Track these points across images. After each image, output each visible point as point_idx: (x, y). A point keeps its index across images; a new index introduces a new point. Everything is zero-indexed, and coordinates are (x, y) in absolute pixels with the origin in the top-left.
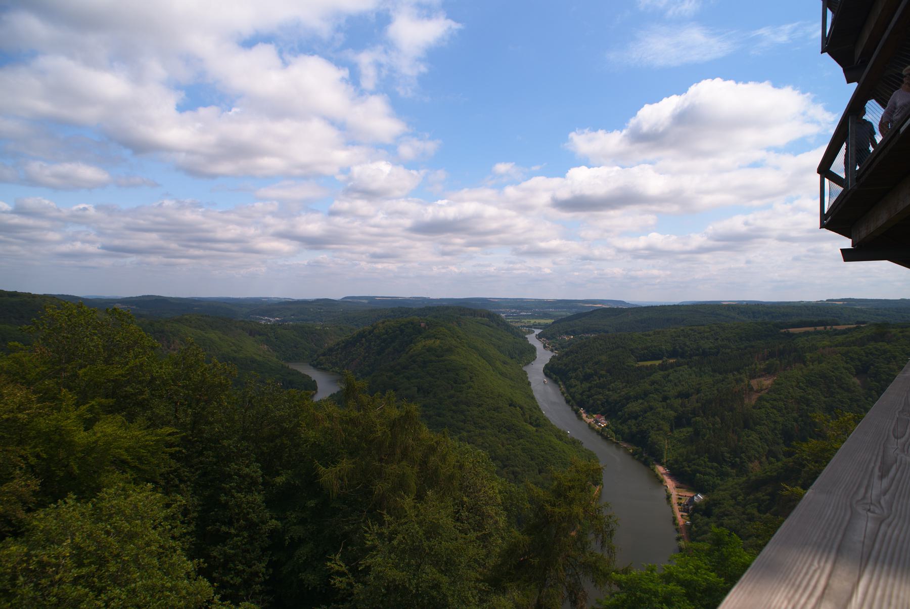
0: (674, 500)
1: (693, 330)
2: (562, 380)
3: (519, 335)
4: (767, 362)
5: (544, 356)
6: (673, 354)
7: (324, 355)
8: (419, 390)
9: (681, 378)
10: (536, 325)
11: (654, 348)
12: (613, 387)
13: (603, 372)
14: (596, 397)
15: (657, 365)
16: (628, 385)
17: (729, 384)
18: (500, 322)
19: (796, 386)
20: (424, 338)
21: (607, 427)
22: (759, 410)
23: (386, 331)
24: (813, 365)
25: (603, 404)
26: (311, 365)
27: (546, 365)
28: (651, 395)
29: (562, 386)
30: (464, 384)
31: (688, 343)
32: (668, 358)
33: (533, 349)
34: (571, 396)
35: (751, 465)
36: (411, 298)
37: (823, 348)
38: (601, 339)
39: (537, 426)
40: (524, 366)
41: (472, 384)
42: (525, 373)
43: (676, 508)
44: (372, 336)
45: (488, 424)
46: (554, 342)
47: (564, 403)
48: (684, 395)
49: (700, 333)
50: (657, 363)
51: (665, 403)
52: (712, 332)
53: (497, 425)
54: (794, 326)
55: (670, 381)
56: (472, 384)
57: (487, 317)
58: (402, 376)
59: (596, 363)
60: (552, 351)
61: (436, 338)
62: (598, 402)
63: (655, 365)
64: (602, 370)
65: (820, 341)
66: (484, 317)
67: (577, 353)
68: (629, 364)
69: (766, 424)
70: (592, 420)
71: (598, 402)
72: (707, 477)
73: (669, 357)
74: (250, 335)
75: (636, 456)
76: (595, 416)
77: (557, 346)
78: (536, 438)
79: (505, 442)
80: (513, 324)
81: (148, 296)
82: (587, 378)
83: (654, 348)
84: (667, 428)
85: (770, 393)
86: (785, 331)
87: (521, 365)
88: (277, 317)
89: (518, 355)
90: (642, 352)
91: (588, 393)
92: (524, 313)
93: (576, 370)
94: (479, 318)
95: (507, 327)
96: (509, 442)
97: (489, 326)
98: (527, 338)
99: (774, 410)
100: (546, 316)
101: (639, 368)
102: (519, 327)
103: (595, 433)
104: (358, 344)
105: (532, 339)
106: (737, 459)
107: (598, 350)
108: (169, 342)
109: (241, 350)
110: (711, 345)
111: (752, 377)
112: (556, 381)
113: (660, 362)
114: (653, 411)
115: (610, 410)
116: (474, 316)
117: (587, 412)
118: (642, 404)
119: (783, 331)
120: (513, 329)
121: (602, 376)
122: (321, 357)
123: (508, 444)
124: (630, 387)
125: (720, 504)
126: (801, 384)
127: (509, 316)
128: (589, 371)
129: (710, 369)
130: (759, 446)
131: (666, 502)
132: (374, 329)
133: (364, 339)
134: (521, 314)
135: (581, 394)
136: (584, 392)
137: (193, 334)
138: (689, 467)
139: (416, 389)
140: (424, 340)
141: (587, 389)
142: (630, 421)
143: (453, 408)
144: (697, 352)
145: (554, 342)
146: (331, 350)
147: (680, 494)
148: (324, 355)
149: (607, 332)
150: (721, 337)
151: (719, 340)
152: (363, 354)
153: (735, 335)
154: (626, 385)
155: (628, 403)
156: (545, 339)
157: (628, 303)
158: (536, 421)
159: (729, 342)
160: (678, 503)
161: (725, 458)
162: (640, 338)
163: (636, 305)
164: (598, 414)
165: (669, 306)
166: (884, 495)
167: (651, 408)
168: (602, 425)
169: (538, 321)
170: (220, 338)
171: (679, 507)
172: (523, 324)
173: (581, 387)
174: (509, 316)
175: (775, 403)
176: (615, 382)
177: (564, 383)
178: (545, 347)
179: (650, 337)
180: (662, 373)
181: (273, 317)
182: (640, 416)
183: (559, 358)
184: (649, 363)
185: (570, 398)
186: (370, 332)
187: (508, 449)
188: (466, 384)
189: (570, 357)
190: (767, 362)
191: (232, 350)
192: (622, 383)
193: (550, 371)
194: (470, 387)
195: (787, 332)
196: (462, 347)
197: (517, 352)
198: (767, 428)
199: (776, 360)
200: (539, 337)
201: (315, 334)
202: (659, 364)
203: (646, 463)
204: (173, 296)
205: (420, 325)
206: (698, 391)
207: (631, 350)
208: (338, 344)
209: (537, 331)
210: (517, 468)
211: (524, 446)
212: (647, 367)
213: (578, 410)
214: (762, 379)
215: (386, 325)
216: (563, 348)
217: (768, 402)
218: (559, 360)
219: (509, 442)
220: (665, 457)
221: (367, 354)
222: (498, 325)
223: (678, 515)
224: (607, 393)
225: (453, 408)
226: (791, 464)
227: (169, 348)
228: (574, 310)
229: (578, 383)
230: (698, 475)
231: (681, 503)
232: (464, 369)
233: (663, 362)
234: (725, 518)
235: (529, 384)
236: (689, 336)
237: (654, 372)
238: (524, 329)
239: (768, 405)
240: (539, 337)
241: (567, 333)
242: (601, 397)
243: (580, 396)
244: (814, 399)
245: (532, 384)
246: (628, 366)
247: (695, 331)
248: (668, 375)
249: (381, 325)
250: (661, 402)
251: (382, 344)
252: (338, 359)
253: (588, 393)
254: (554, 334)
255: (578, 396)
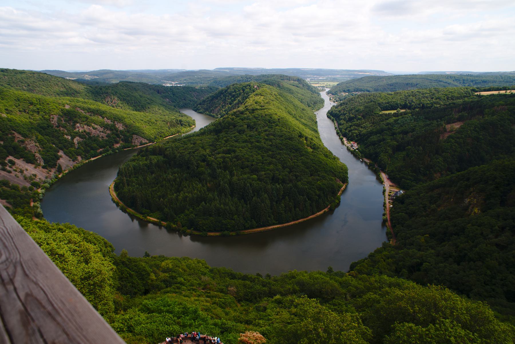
0: (387, 193)
1: (419, 92)
2: (336, 120)
3: (315, 92)
4: (460, 114)
5: (329, 105)
6: (404, 107)
7: (200, 104)
8: (248, 127)
9: (405, 122)
10: (327, 86)
11: (393, 103)
12: (364, 126)
13: (360, 117)
14: (353, 131)
15: (393, 113)
16: (373, 125)
17: (433, 127)
18: (305, 84)
19: (473, 130)
20: (255, 95)
21: (357, 149)
22: (447, 144)
23: (235, 90)
24: (488, 117)
25: (357, 136)
26: (193, 110)
27: (329, 111)
28: (385, 132)
29: (336, 124)
30: (274, 123)
31: (414, 101)
32: (400, 109)
33: (322, 101)
34: (340, 130)
35: (435, 175)
36: (255, 68)
37: (498, 106)
38: (362, 96)
39: (314, 148)
40: (316, 111)
41: (278, 123)
42: (315, 116)
43: (387, 197)
44: (227, 93)
45: (284, 147)
46: (336, 97)
47: (335, 134)
48: (405, 133)
49: (423, 94)
50: (393, 112)
51: (392, 137)
52: (431, 94)
53: (289, 148)
54: (485, 90)
55: (399, 124)
56: (278, 123)
57: (297, 81)
58: (239, 118)
59: (357, 111)
60: (334, 102)
61: (261, 95)
62: (355, 134)
63: (391, 113)
64: (359, 115)
65: (498, 101)
66: (295, 81)
67: (347, 104)
68: (375, 112)
69: (450, 152)
70: (350, 145)
71: (355, 134)
72: (408, 181)
73: (401, 109)
74: (159, 93)
75: (371, 167)
76: (351, 142)
77: (337, 99)
78: (311, 156)
79: (293, 158)
80: (312, 85)
81: (103, 70)
82: (350, 119)
83: (393, 103)
84: (390, 152)
85: (456, 134)
86: (477, 94)
87: (314, 110)
88: (176, 81)
89: (313, 105)
90: (385, 105)
91: (349, 129)
92: (321, 78)
93: (345, 115)
94: (292, 82)
95: (309, 88)
96: (295, 158)
97: (297, 87)
98: (320, 94)
99: (456, 144)
100: (334, 80)
101: (381, 115)
102: (317, 87)
103: (350, 153)
104: (219, 98)
105: (324, 95)
106: (428, 172)
107: (359, 103)
108: (111, 99)
109: (153, 103)
110: (428, 102)
111: (448, 123)
112: (333, 121)
113: (395, 111)
114: (384, 141)
115: (360, 139)
116: (289, 81)
117: (348, 140)
118: (379, 137)
119: (476, 94)
120: (312, 89)
121: (359, 119)
122: (199, 106)
123: (294, 159)
124: (374, 126)
125: (410, 197)
126: (477, 129)
127: (312, 80)
128: (352, 115)
129: (424, 117)
130: (442, 165)
131: (382, 194)
132: (228, 89)
133: (222, 95)
134: (320, 78)
135: (346, 129)
136: (347, 128)
137: (124, 94)
138: (399, 175)
139: (246, 126)
140: (254, 96)
141: (349, 127)
142: (370, 146)
143: (266, 137)
144: (419, 106)
145: (336, 97)
146: (204, 101)
147: (391, 190)
148: (200, 104)
149: (369, 91)
150: (436, 97)
151: (434, 99)
152: (222, 104)
153: (444, 96)
154: (372, 125)
155: (371, 136)
156: (331, 95)
157: (386, 72)
158: (313, 146)
159: (440, 100)
160: (389, 195)
161: (421, 171)
162: (385, 96)
163: (391, 74)
164: (353, 141)
165: (410, 75)
166: (141, 310)
167: (384, 140)
168: (355, 148)
169: (329, 83)
170: (140, 96)
171: (389, 197)
172: (319, 85)
173: (346, 125)
174: (312, 80)
175: (458, 140)
176: (366, 123)
177: (337, 122)
178: (330, 99)
179: (391, 96)
180: (394, 118)
181: (174, 81)
182: (376, 144)
183: (336, 107)
184: (387, 112)
185: (339, 131)
186: (226, 91)
187: (294, 162)
188: (275, 124)
189: (342, 107)
190: (460, 114)
191: (147, 103)
192: (370, 124)
193: (331, 115)
194: (277, 125)
195: (479, 94)
196: (277, 101)
197: (312, 103)
198: (449, 155)
199: (466, 113)
200: (328, 93)
201: (196, 92)
202: (394, 113)
203: (376, 173)
204: (117, 70)
205: (254, 87)
206: (413, 130)
207: (379, 104)
208: (208, 98)
209: (327, 90)
210: (297, 173)
211: (303, 161)
212: (386, 115)
213: (343, 139)
214: (454, 124)
215: (235, 87)
216: (341, 100)
217: (454, 139)
218: (336, 108)
219: (295, 158)
220: (387, 168)
221: (224, 104)
222: (303, 86)
223: (387, 201)
224: (361, 129)
225: (266, 137)
226: (454, 178)
227: (112, 103)
228: (352, 76)
229: (345, 122)
230: (403, 179)
231: (390, 195)
232: (276, 114)
233: (397, 111)
234: (411, 205)
235: (316, 122)
236: (416, 96)
237: (390, 118)
238: (319, 89)
239: (453, 141)
240: (328, 93)
241: (344, 91)
242: (357, 132)
243: (344, 131)
244: (483, 138)
245: (318, 122)
246: (375, 114)
247: (420, 93)
248: (398, 120)
249: (232, 87)
250: (390, 136)
251: (232, 98)
252: (208, 107)
253: (349, 129)
254: (337, 92)
255: (343, 130)
